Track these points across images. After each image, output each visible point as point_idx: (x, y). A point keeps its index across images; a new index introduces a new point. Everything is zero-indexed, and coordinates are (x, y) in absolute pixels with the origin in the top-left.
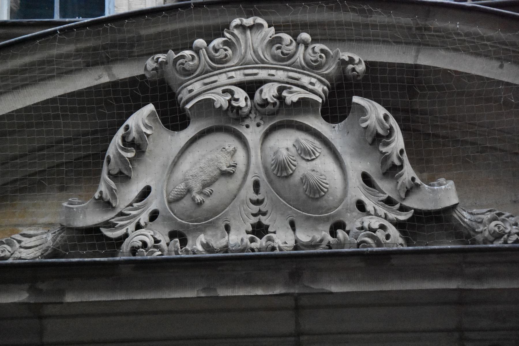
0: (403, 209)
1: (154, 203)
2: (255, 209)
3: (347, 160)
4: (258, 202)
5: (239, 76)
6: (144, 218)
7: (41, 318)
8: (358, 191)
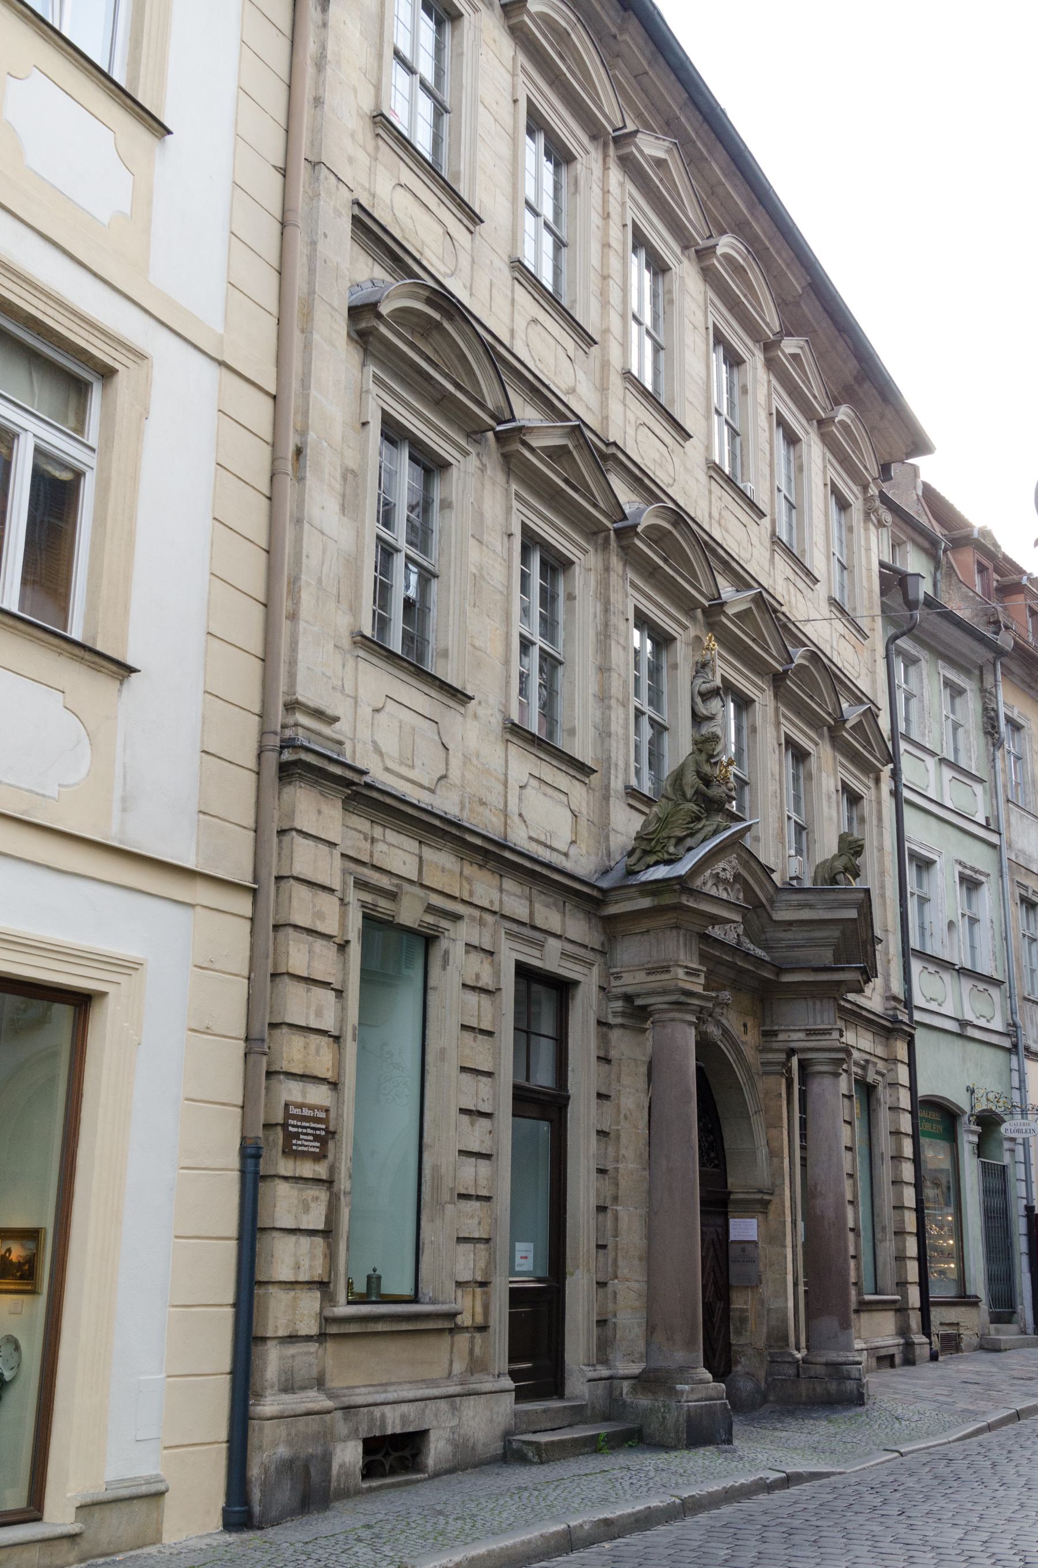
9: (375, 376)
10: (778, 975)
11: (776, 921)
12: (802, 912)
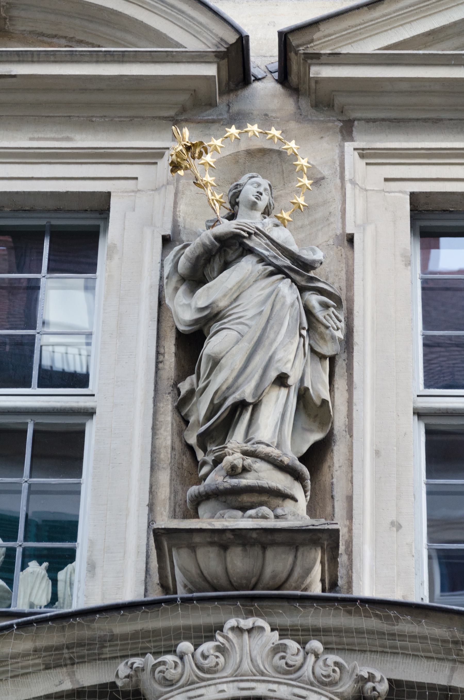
9: (363, 154)
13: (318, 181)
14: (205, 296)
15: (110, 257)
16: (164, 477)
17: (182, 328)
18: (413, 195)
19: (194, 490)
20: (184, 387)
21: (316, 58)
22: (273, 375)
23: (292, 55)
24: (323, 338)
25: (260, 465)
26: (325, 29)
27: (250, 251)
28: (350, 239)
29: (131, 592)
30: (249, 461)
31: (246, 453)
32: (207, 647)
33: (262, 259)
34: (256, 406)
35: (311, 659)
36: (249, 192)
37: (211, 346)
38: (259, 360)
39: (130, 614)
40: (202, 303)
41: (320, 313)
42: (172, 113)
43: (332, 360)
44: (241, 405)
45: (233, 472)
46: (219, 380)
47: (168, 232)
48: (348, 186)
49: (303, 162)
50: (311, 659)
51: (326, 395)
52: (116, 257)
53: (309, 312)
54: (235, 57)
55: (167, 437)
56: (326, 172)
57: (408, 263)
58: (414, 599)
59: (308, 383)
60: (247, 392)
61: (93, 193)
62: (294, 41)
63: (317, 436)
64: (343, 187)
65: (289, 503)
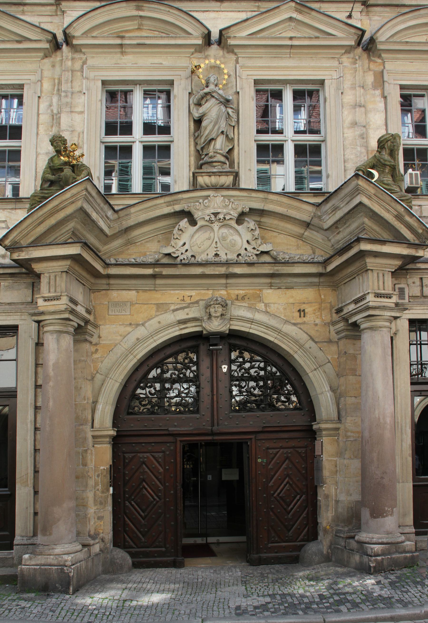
0: (258, 250)
1: (186, 247)
2: (216, 250)
3: (243, 236)
4: (216, 248)
5: (213, 211)
6: (184, 251)
7: (271, 283)
8: (246, 245)
10: (325, 268)
11: (326, 230)
12: (336, 215)
13: (229, 76)
14: (202, 110)
15: (174, 98)
16: (192, 159)
17: (195, 118)
18: (254, 80)
19: (201, 162)
20: (196, 134)
21: (229, 37)
22: (220, 131)
23: (223, 37)
24: (231, 120)
25: (218, 156)
26: (232, 29)
27: (213, 97)
28: (238, 93)
29: (185, 189)
30: (215, 154)
31: (214, 152)
32: (206, 201)
33: (217, 99)
34: (216, 139)
35: (231, 203)
36: (212, 80)
37: (204, 124)
38: (216, 127)
39: (332, 516)
40: (201, 112)
41: (231, 113)
42: (189, 55)
43: (234, 127)
44: (212, 139)
45: (211, 157)
46: (207, 132)
47: (190, 91)
48: (238, 77)
49: (226, 71)
50: (231, 203)
51: (233, 136)
52: (177, 99)
53: (228, 114)
54: (207, 37)
55: (192, 148)
56: (232, 73)
57: (253, 100)
58: (254, 188)
59: (228, 133)
60: (213, 136)
61: (169, 80)
62: (223, 33)
63: (231, 147)
64: (236, 78)
65: (225, 165)
